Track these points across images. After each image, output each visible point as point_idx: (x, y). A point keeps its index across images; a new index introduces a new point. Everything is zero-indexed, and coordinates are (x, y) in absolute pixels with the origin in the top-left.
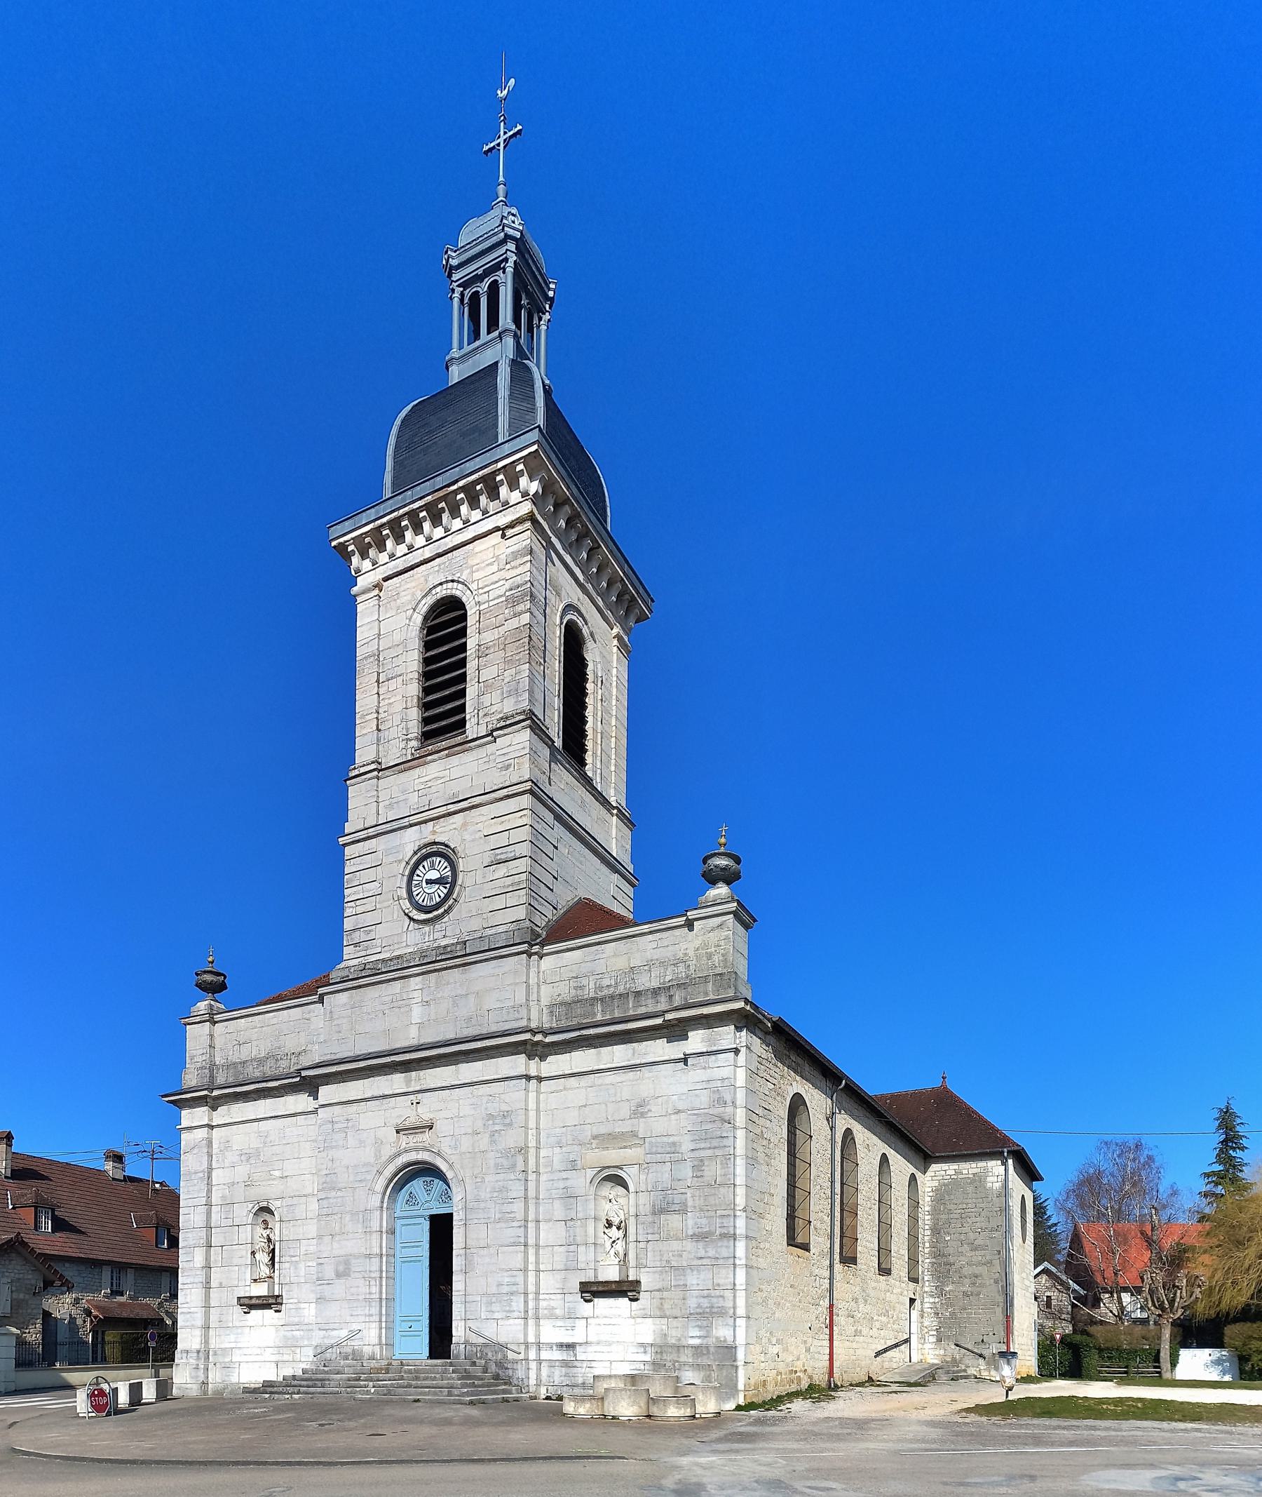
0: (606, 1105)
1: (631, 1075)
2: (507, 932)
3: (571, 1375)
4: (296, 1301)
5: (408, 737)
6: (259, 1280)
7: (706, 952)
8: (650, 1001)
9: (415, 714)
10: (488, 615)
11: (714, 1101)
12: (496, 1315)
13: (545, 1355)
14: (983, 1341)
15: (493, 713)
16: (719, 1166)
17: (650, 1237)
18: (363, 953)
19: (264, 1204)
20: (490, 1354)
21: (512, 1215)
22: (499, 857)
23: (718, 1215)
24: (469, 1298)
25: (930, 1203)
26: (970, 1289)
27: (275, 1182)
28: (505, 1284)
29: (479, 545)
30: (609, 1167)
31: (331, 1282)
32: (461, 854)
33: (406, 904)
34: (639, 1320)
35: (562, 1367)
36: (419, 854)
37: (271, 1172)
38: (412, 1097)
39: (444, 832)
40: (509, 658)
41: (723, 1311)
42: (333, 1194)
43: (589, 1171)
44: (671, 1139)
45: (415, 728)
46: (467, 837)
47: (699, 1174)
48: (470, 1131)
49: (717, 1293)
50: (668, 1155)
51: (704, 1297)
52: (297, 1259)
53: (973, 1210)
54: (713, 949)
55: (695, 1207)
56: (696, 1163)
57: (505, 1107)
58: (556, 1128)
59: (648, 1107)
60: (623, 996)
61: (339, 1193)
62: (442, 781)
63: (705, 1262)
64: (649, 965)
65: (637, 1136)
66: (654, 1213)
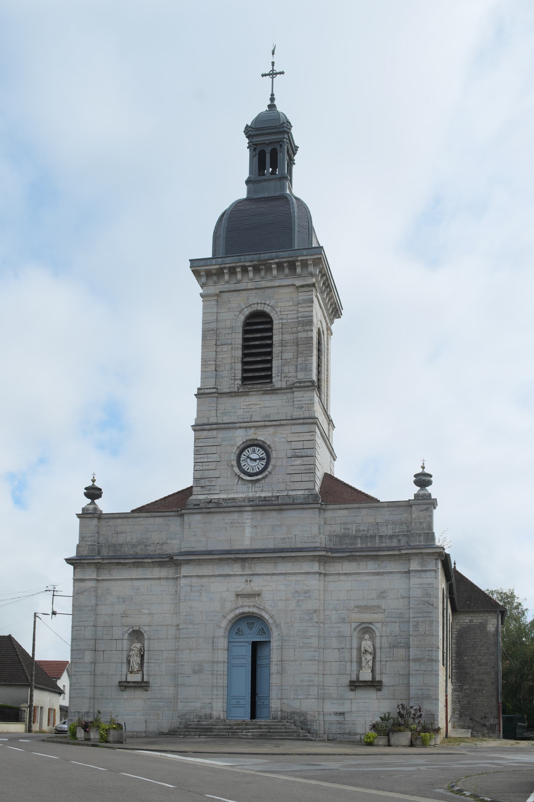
0: (363, 591)
1: (377, 577)
2: (304, 495)
3: (342, 728)
4: (159, 685)
5: (235, 378)
6: (133, 672)
7: (419, 521)
8: (388, 541)
9: (239, 366)
10: (287, 326)
11: (424, 594)
12: (300, 697)
13: (327, 718)
14: (485, 717)
15: (290, 377)
16: (427, 626)
17: (388, 659)
18: (208, 492)
19: (137, 628)
20: (296, 717)
21: (310, 645)
22: (297, 454)
23: (426, 650)
24: (284, 688)
25: (455, 638)
26: (478, 688)
27: (143, 616)
28: (306, 680)
29: (281, 290)
30: (365, 623)
31: (189, 675)
32: (273, 448)
33: (236, 470)
34: (381, 701)
35: (337, 724)
36: (245, 444)
37: (141, 610)
38: (246, 577)
39: (262, 436)
40: (301, 352)
41: (429, 697)
42: (191, 626)
43: (353, 624)
44: (400, 611)
45: (239, 374)
46: (276, 440)
47: (416, 629)
48: (284, 599)
49: (426, 688)
50: (398, 619)
51: (418, 690)
52: (160, 661)
53: (479, 643)
54: (423, 520)
55: (414, 645)
56: (415, 624)
57: (305, 588)
58: (333, 600)
59: (387, 594)
60: (373, 537)
61: (195, 626)
62: (259, 406)
63: (419, 672)
64: (387, 523)
65: (381, 608)
66: (390, 648)
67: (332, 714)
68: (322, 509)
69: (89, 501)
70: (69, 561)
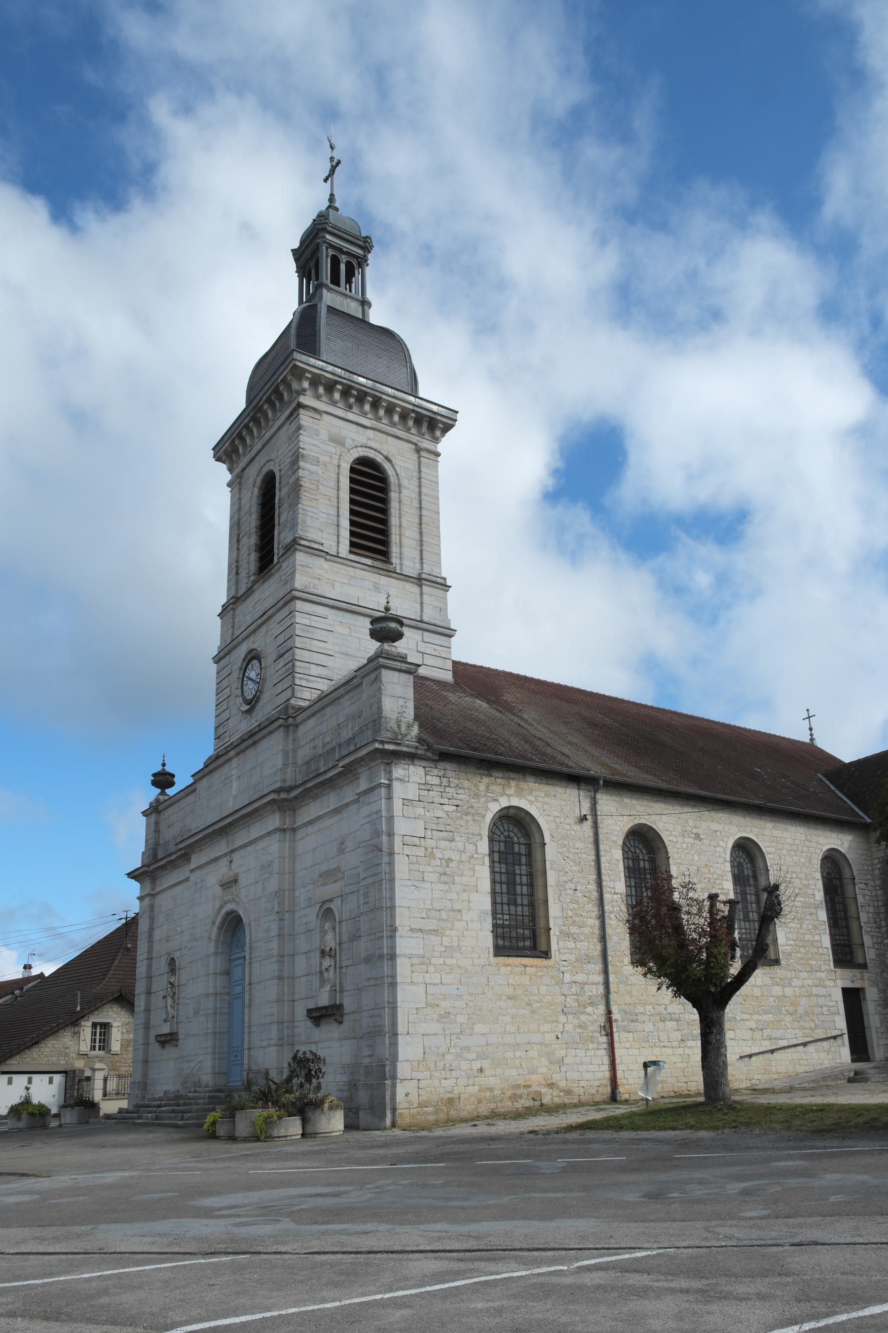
67: (29, 1086)
68: (291, 725)
69: (159, 791)
70: (133, 875)
